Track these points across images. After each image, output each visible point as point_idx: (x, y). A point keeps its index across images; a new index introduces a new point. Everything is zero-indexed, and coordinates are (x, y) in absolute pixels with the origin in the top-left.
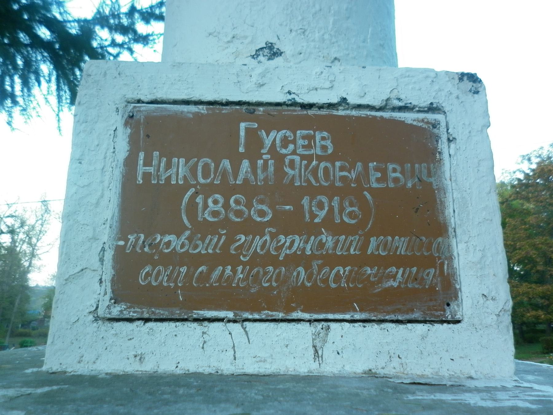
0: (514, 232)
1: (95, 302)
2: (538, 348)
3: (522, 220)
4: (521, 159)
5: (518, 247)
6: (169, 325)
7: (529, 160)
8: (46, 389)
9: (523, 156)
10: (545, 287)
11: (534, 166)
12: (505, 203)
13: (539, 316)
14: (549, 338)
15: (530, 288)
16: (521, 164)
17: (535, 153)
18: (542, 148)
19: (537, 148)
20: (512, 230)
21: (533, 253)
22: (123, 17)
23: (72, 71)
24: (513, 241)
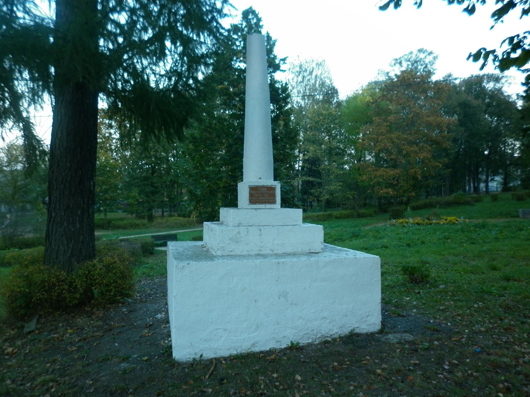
0: (379, 128)
1: (156, 71)
2: (387, 216)
3: (386, 118)
4: (394, 62)
5: (380, 140)
6: (378, 79)
7: (400, 63)
8: (443, 192)
9: (396, 60)
10: (396, 171)
11: (404, 69)
12: (375, 104)
13: (389, 193)
14: (395, 208)
15: (386, 172)
16: (394, 66)
17: (406, 57)
18: (411, 53)
19: (407, 52)
20: (377, 126)
21: (389, 146)
22: (7, 336)
23: (22, 6)
24: (376, 135)
